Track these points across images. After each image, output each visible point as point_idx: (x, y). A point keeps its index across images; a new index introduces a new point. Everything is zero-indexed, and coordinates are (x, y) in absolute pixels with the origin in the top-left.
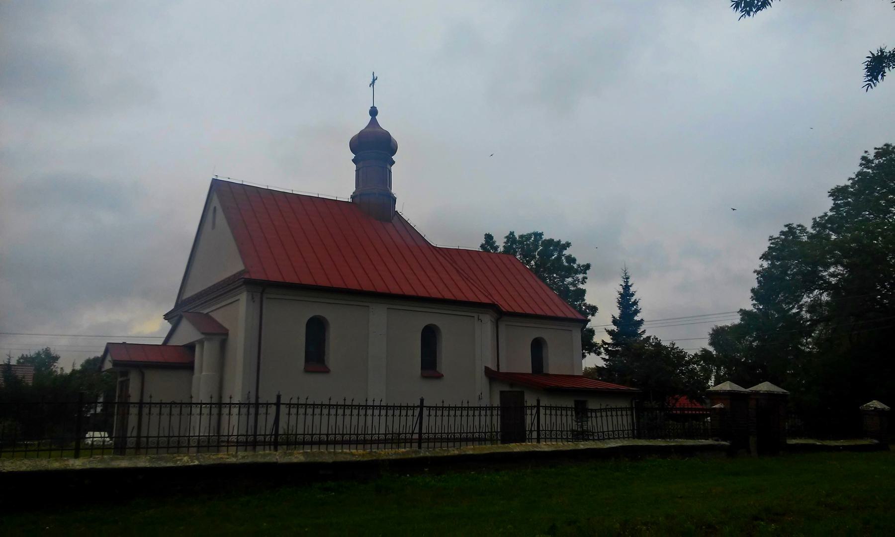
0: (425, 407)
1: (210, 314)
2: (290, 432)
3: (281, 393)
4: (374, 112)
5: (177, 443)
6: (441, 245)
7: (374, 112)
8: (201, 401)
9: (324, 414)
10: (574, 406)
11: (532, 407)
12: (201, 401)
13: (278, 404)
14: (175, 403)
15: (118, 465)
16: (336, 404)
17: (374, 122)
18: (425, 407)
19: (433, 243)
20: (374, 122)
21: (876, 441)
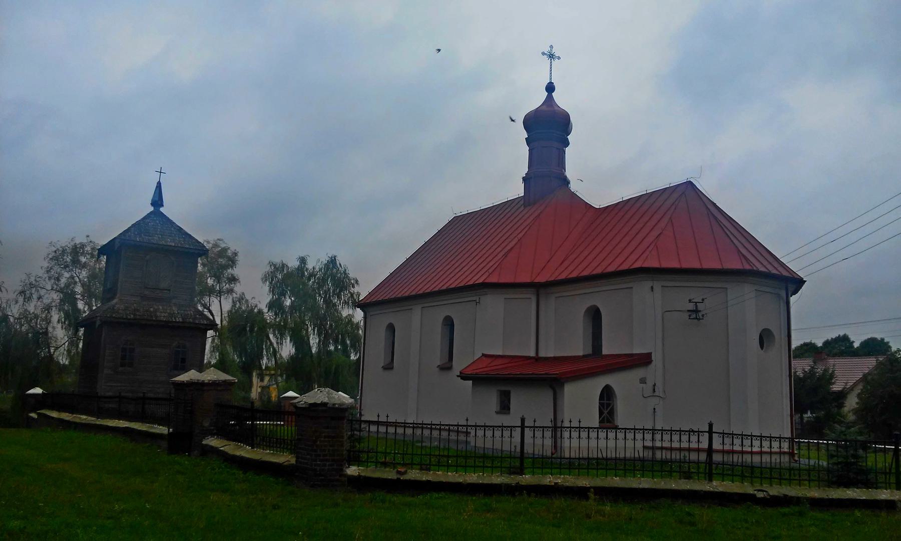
0: (527, 427)
1: (793, 346)
2: (591, 456)
3: (525, 416)
4: (550, 88)
5: (801, 474)
6: (587, 200)
7: (550, 88)
8: (733, 431)
9: (591, 438)
10: (788, 434)
11: (467, 429)
12: (733, 431)
13: (523, 427)
14: (693, 431)
15: (114, 422)
16: (430, 423)
17: (549, 100)
18: (527, 427)
19: (587, 200)
20: (549, 100)
21: (314, 350)
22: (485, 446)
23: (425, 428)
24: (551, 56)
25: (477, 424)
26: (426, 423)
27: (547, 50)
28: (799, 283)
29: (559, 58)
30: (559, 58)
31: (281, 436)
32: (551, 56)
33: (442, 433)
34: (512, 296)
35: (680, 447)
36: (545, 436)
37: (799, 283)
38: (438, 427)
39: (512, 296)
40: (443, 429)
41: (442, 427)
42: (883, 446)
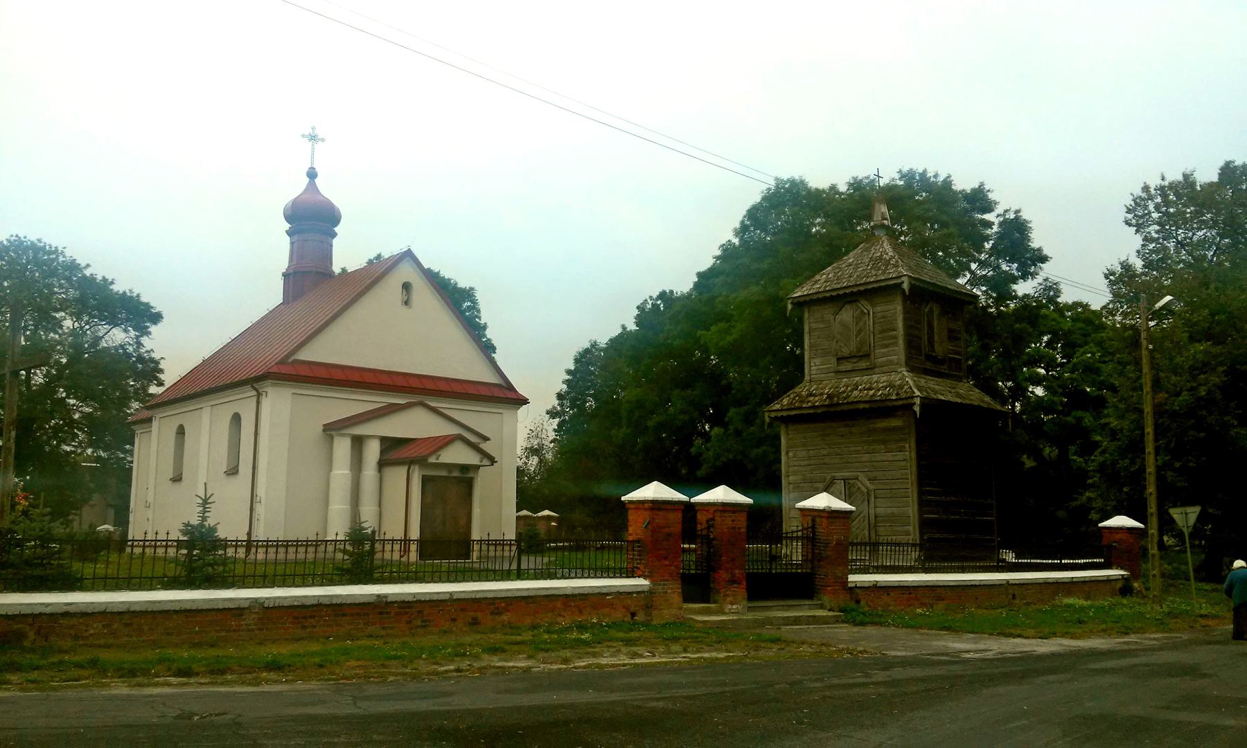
4: (312, 174)
7: (312, 174)
17: (312, 186)
20: (312, 186)
22: (393, 559)
23: (290, 545)
24: (313, 138)
25: (135, 539)
26: (241, 539)
27: (308, 131)
28: (156, 318)
29: (303, 136)
30: (303, 136)
31: (776, 553)
32: (313, 138)
33: (505, 548)
34: (172, 413)
35: (83, 564)
36: (327, 550)
37: (156, 318)
38: (164, 543)
39: (172, 413)
40: (310, 545)
41: (170, 543)
42: (1063, 561)
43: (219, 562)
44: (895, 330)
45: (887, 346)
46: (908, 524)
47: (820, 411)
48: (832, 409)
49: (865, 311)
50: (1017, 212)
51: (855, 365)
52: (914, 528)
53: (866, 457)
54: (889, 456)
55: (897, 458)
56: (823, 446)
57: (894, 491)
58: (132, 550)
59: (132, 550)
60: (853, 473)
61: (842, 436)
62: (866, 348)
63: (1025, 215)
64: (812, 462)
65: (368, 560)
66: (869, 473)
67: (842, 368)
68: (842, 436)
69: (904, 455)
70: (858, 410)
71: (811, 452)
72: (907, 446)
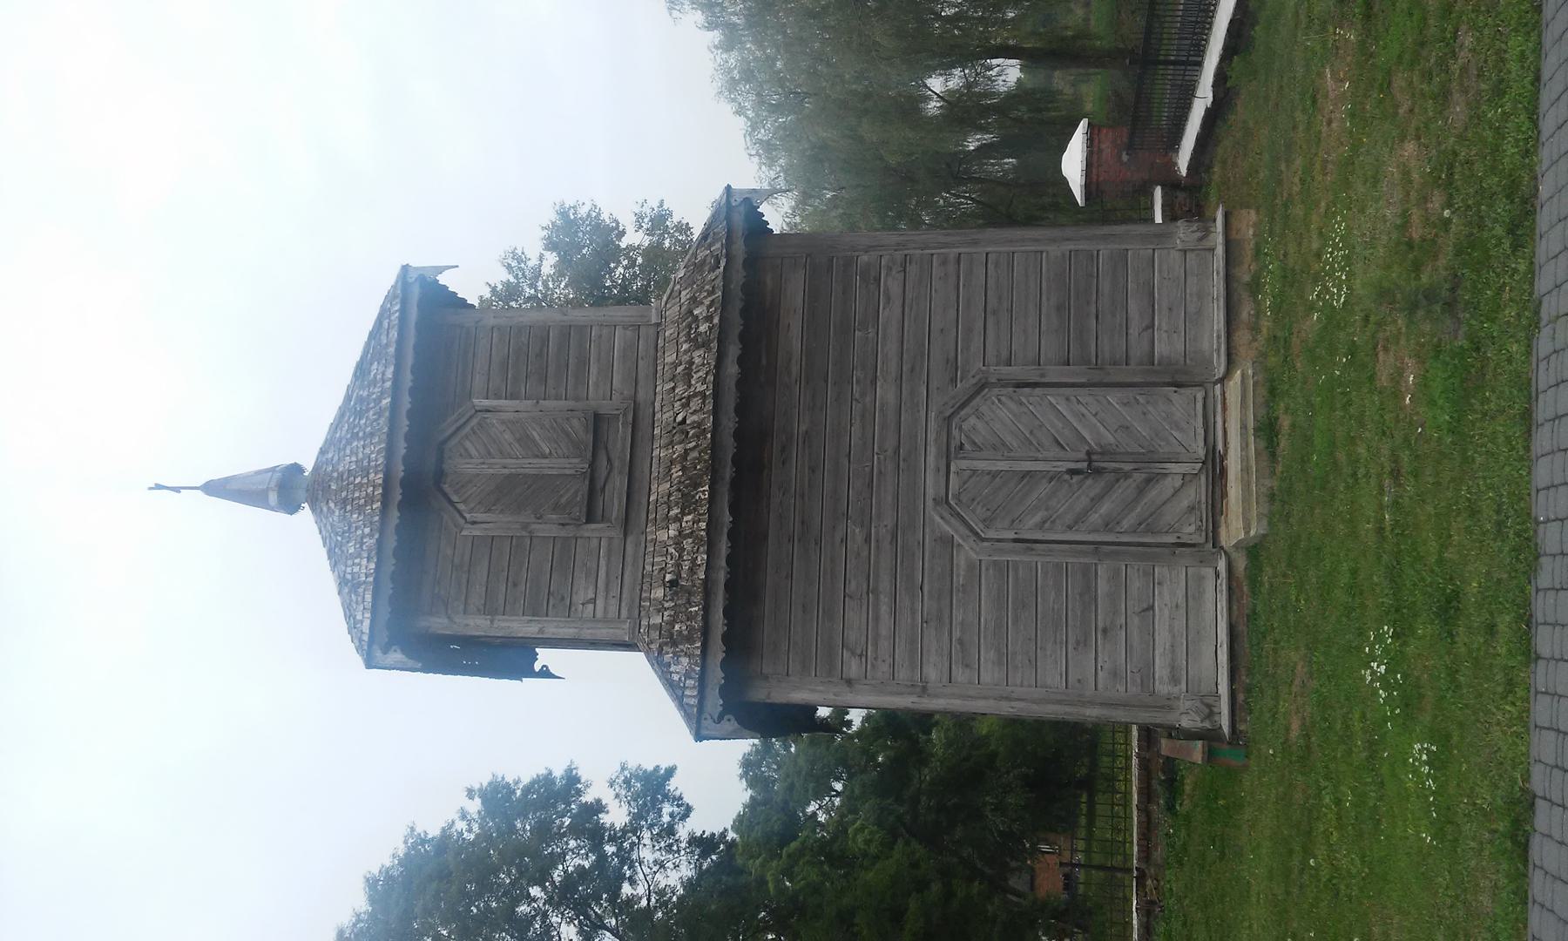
43: (873, 850)
44: (545, 340)
45: (583, 362)
46: (1093, 257)
47: (727, 518)
48: (728, 472)
49: (474, 421)
50: (470, 793)
51: (616, 464)
52: (1105, 238)
53: (886, 392)
54: (889, 315)
55: (895, 289)
56: (839, 535)
57: (992, 302)
58: (1113, 746)
59: (1113, 746)
60: (931, 437)
61: (813, 470)
62: (577, 427)
63: (482, 779)
64: (885, 584)
65: (1484, 478)
66: (934, 384)
67: (616, 508)
68: (813, 470)
69: (890, 269)
70: (741, 383)
71: (853, 586)
72: (865, 258)
